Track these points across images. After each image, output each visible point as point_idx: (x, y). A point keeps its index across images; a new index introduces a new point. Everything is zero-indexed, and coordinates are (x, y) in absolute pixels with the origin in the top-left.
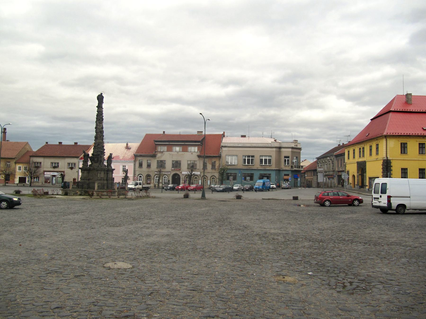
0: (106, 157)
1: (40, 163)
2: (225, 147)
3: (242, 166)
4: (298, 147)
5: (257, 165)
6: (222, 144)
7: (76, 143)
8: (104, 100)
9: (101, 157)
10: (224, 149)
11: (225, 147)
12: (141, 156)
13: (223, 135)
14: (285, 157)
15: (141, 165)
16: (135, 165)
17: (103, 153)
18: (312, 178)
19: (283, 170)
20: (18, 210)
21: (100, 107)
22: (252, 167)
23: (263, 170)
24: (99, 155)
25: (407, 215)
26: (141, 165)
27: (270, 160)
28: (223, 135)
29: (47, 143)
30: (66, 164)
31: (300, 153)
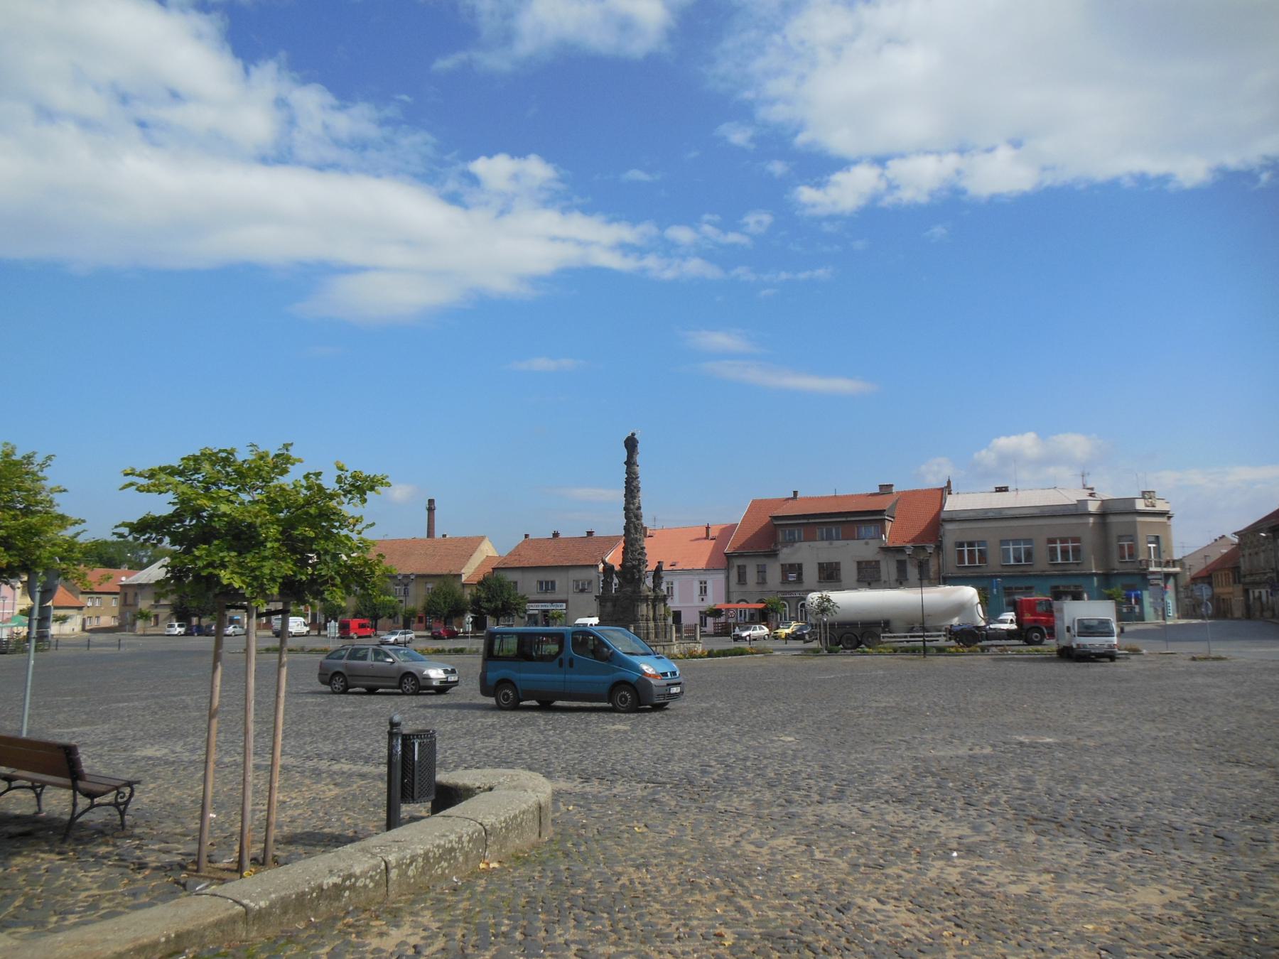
0: (651, 567)
1: (516, 583)
2: (952, 521)
3: (1000, 569)
4: (1160, 507)
5: (1041, 562)
6: (943, 516)
7: (590, 533)
8: (640, 447)
9: (640, 571)
10: (948, 527)
11: (952, 521)
12: (741, 556)
13: (948, 489)
14: (1120, 538)
15: (742, 580)
16: (728, 578)
17: (642, 562)
18: (1230, 589)
19: (1117, 574)
20: (1096, 669)
21: (630, 463)
22: (1029, 569)
23: (1058, 576)
24: (634, 567)
25: (383, 697)
26: (742, 580)
27: (1077, 551)
28: (948, 489)
29: (526, 536)
30: (571, 583)
31: (1166, 527)
